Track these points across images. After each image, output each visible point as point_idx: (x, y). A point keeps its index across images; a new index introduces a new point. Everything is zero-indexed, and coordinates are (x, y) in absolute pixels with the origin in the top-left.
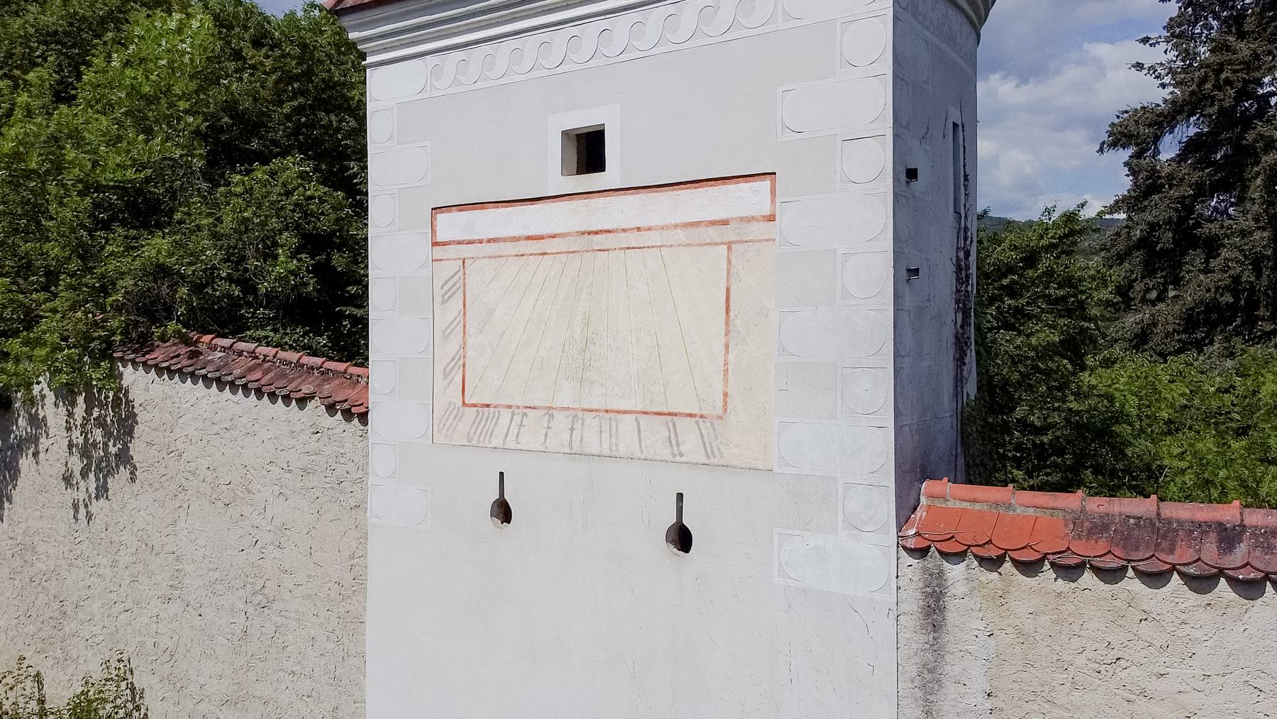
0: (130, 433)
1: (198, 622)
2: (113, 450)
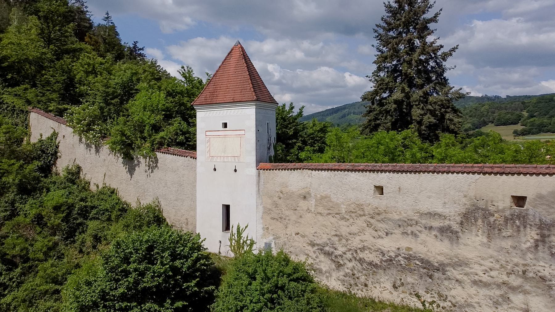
0: (158, 162)
1: (170, 190)
2: (154, 165)
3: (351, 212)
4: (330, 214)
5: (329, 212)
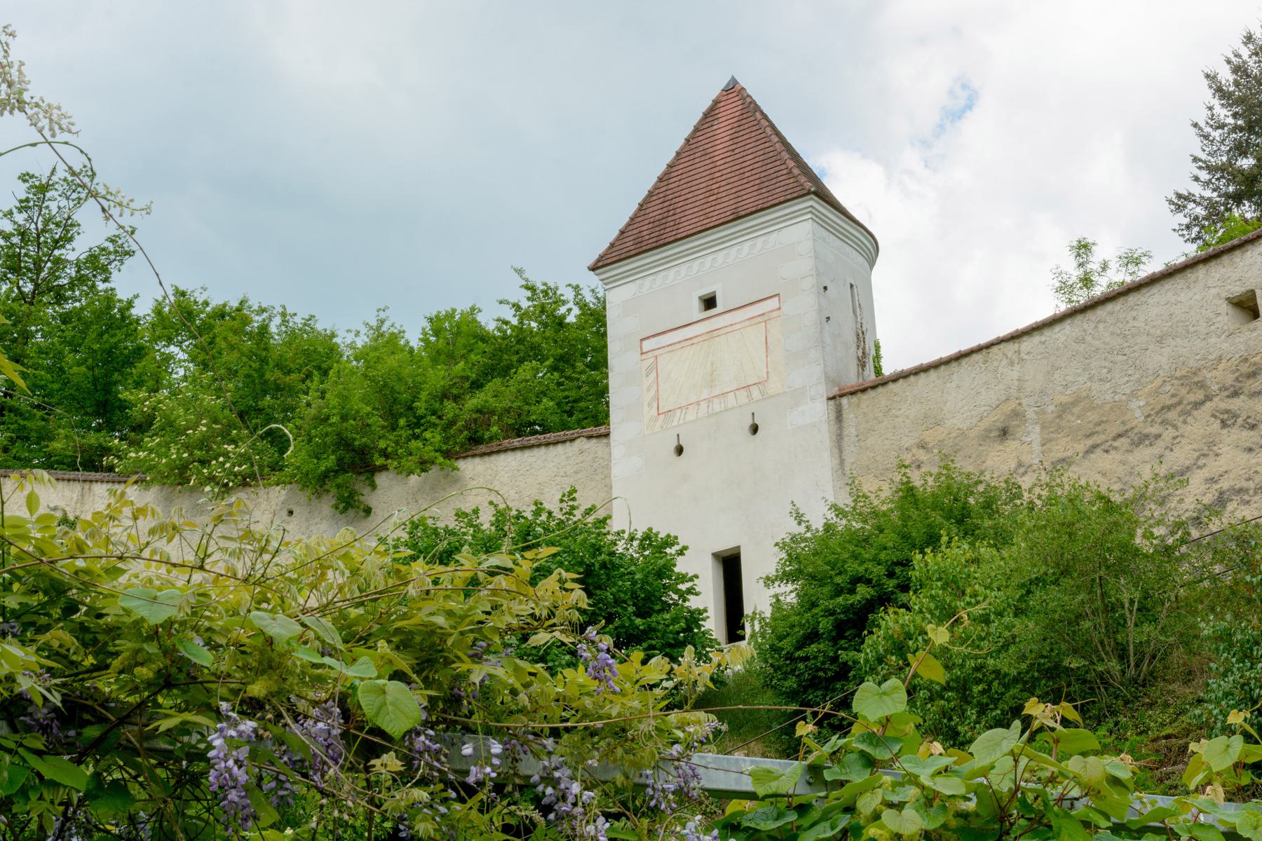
3: (1163, 408)
4: (1095, 447)
5: (1090, 442)
